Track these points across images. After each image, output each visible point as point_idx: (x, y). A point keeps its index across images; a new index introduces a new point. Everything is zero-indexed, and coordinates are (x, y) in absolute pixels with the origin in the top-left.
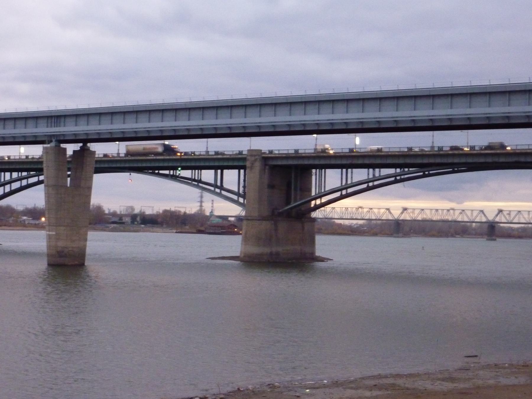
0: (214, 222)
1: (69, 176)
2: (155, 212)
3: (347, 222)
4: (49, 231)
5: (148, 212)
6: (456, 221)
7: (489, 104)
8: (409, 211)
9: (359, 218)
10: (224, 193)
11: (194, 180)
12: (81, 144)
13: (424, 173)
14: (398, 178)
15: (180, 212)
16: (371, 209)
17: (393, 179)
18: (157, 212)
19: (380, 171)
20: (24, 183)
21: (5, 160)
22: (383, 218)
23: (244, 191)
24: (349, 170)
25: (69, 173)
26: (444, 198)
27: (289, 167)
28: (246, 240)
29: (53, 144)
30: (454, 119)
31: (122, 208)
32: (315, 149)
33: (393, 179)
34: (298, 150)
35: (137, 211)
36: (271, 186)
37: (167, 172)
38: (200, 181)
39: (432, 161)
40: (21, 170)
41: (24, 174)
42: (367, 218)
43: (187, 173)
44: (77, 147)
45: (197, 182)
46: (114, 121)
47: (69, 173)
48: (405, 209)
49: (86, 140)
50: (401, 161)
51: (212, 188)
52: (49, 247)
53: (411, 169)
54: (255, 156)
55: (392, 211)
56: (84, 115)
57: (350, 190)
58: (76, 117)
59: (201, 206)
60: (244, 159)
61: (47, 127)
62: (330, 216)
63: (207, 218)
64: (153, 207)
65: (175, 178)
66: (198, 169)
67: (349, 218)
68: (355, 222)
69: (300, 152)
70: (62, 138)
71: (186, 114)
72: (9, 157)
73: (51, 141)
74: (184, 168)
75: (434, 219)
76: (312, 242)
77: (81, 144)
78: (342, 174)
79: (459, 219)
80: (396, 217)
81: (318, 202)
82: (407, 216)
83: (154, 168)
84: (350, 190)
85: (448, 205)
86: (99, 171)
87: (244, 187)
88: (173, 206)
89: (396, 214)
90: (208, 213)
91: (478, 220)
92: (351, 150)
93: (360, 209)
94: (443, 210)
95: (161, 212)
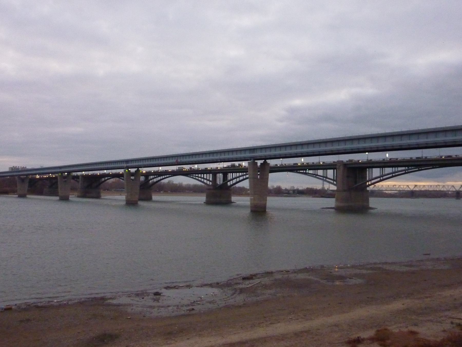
0: (329, 192)
1: (259, 175)
2: (303, 189)
3: (390, 192)
4: (251, 197)
5: (300, 188)
6: (440, 191)
7: (280, 150)
8: (418, 186)
9: (394, 190)
10: (327, 180)
11: (314, 174)
12: (264, 160)
13: (419, 169)
14: (407, 171)
15: (314, 188)
16: (400, 186)
17: (404, 172)
18: (304, 188)
19: (398, 169)
20: (245, 177)
21: (442, 159)
22: (405, 190)
23: (336, 179)
24: (384, 168)
25: (259, 173)
26: (435, 181)
27: (357, 168)
28: (337, 200)
29: (252, 161)
30: (428, 143)
31: (290, 187)
32: (367, 160)
33: (404, 172)
34: (412, 158)
35: (295, 188)
36: (348, 177)
37: (302, 171)
38: (317, 175)
39: (422, 163)
40: (243, 172)
41: (245, 173)
42: (398, 190)
43: (311, 172)
44: (262, 161)
45: (316, 176)
46: (225, 154)
47: (259, 173)
48: (416, 186)
49: (265, 159)
50: (407, 164)
51: (322, 178)
52: (251, 204)
53: (412, 167)
54: (340, 163)
55: (410, 187)
56: (264, 148)
57: (384, 177)
58: (199, 155)
59: (323, 186)
60: (336, 165)
61: (249, 154)
62: (381, 189)
63: (326, 191)
64: (302, 186)
65: (306, 174)
66: (315, 170)
67: (389, 190)
68: (393, 192)
69: (428, 158)
70: (255, 158)
71: (318, 145)
72: (285, 164)
73: (251, 160)
74: (309, 169)
75: (430, 190)
76: (368, 201)
77: (264, 160)
78: (380, 170)
79: (442, 190)
80: (412, 189)
81: (370, 183)
82: (417, 189)
83: (297, 170)
84: (384, 177)
85: (436, 184)
86: (272, 171)
87: (336, 177)
88: (310, 186)
89: (412, 188)
90: (326, 189)
91: (451, 190)
92: (384, 160)
93: (395, 186)
94: (434, 186)
95: (306, 188)
